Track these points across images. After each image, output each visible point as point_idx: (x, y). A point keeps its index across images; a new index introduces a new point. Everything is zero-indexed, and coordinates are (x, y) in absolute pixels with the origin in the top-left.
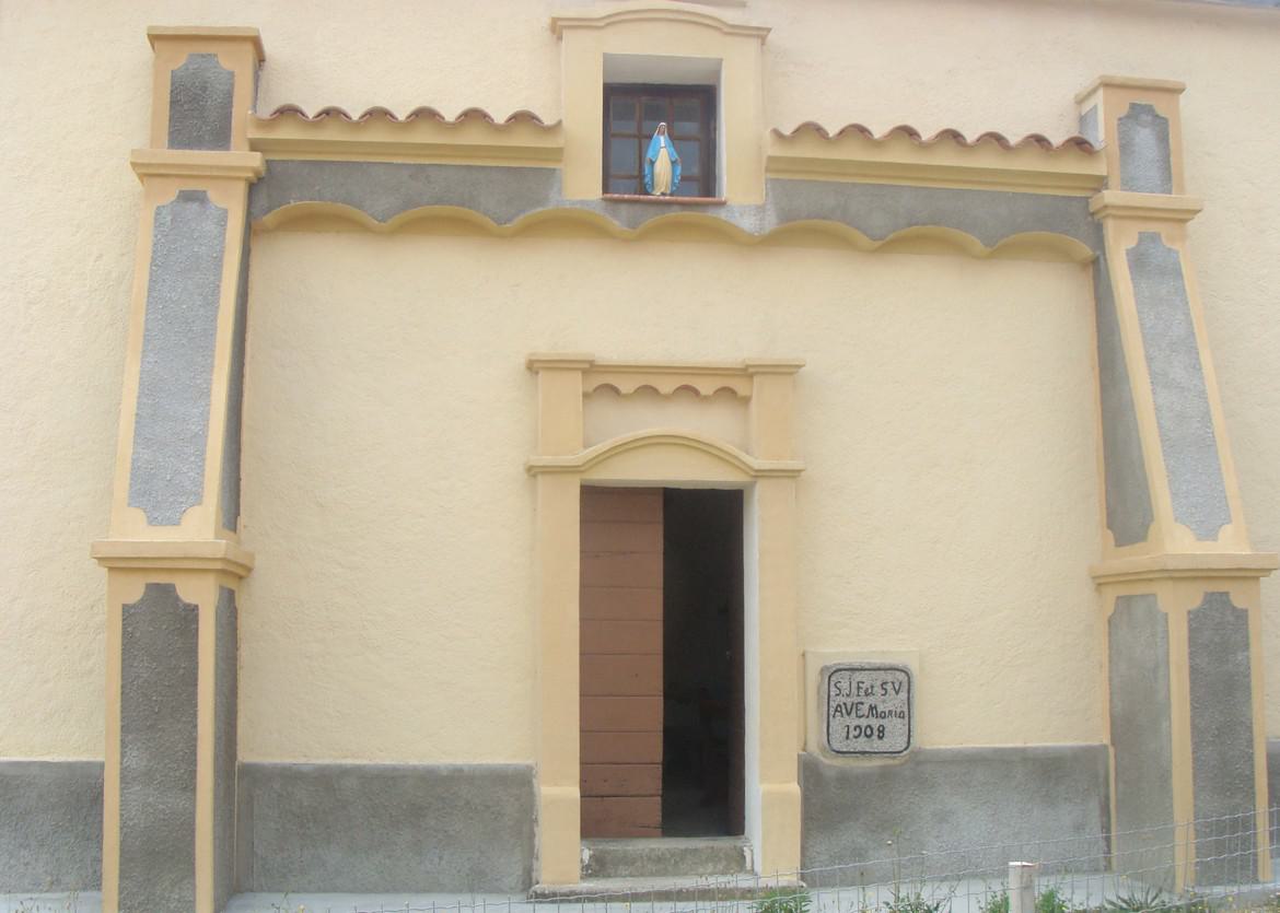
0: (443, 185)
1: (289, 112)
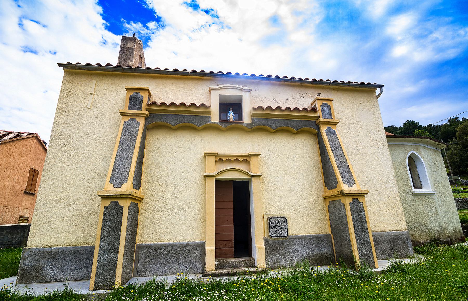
0: (186, 119)
1: (154, 103)
